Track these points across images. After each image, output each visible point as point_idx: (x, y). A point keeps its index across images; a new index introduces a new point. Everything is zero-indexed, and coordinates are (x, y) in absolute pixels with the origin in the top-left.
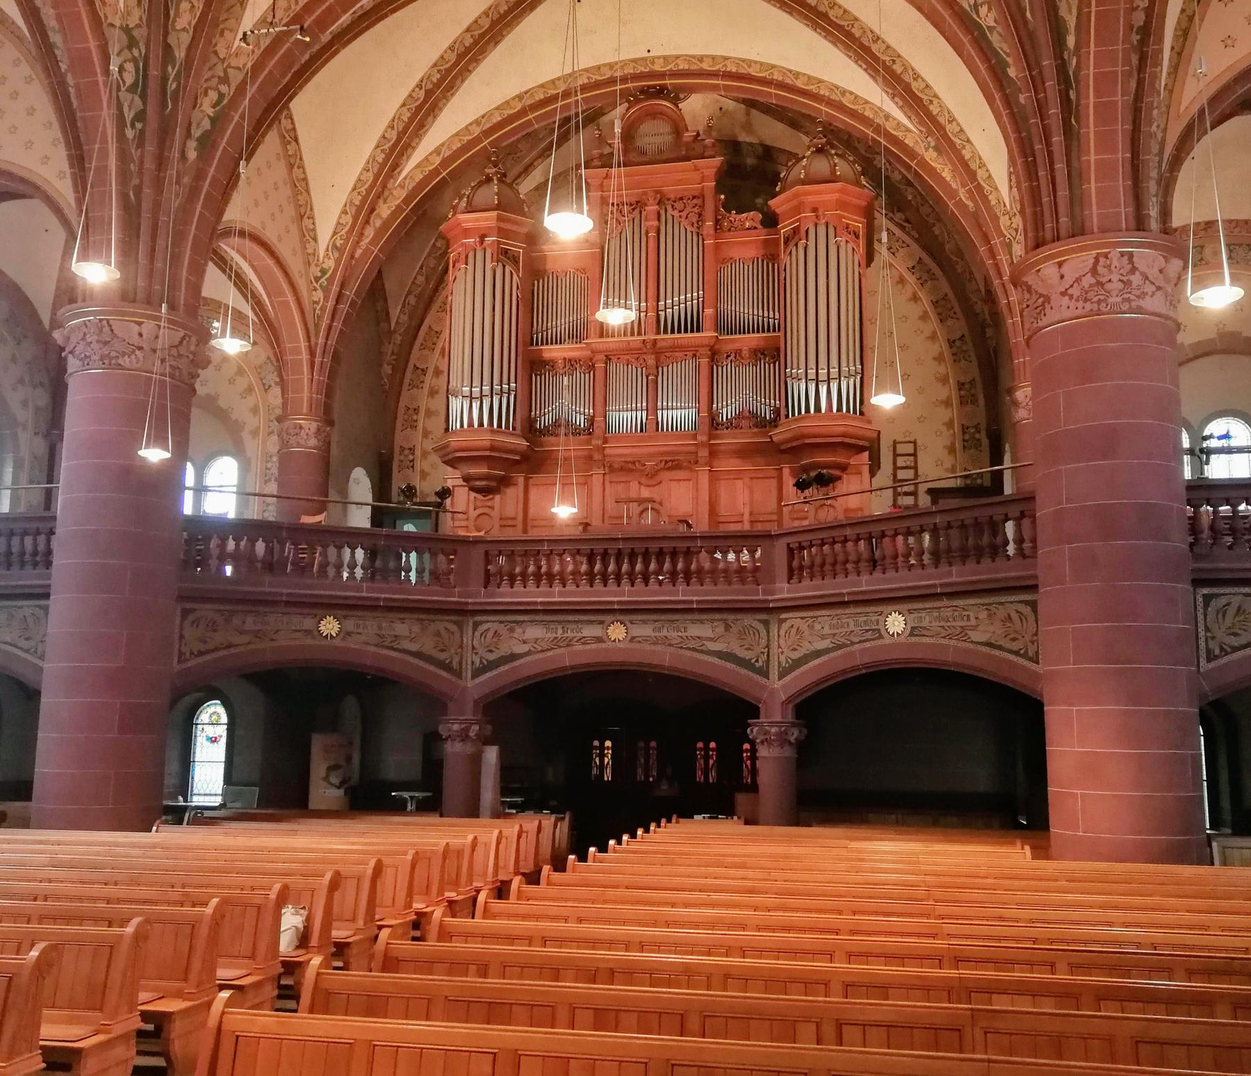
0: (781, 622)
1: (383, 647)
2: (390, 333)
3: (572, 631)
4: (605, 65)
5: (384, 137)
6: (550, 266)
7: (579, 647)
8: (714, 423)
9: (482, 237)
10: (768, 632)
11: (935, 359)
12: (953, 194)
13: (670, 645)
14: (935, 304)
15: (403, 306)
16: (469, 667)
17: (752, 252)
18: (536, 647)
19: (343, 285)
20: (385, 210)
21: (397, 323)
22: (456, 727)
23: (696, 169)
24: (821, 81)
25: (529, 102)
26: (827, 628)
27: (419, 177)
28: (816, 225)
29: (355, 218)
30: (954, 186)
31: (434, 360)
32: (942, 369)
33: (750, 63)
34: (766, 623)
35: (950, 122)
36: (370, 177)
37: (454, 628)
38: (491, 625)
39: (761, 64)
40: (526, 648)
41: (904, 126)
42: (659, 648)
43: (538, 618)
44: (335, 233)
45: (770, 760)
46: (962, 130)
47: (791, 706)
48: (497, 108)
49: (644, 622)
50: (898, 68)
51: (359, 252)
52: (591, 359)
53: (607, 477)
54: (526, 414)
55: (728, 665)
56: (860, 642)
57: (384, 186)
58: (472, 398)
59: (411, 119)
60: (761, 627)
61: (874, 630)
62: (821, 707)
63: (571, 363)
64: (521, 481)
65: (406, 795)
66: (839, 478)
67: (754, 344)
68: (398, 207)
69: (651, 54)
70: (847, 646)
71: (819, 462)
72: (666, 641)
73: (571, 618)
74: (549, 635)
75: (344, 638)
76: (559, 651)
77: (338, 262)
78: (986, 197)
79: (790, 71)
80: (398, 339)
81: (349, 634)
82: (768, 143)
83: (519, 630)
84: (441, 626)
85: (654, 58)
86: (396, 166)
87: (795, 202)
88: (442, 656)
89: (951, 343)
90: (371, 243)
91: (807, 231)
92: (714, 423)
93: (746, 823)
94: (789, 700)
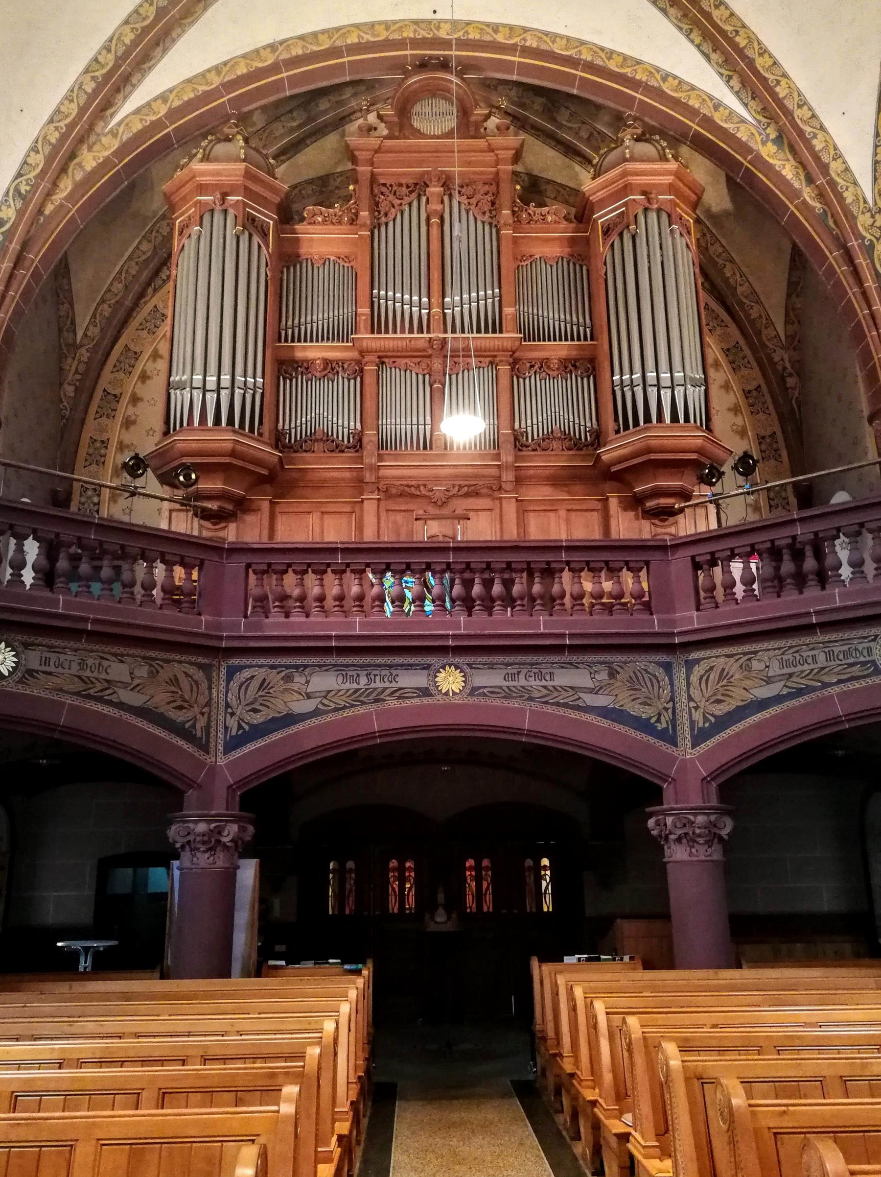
0: (690, 665)
1: (89, 697)
2: (74, 347)
3: (382, 680)
4: (380, 23)
5: (96, 60)
6: (303, 250)
7: (393, 703)
9: (224, 195)
10: (672, 684)
11: (729, 409)
12: (795, 194)
13: (531, 699)
15: (94, 316)
16: (221, 735)
17: (555, 251)
18: (323, 703)
19: (25, 245)
20: (89, 160)
21: (85, 335)
22: (202, 827)
23: (491, 149)
24: (638, 62)
25: (285, 56)
26: (775, 665)
27: (137, 126)
28: (646, 210)
29: (49, 160)
30: (796, 185)
31: (131, 384)
32: (739, 421)
33: (554, 37)
34: (668, 668)
35: (800, 106)
36: (73, 109)
37: (199, 675)
38: (256, 670)
39: (568, 39)
40: (309, 706)
42: (514, 704)
43: (329, 660)
44: (19, 175)
45: (688, 863)
46: (814, 116)
47: (714, 784)
48: (244, 56)
49: (491, 666)
50: (741, 41)
51: (49, 209)
52: (359, 362)
53: (382, 503)
55: (618, 727)
56: (840, 682)
57: (91, 128)
59: (135, 43)
60: (660, 672)
61: (863, 664)
62: (758, 782)
63: (330, 367)
64: (265, 506)
65: (77, 945)
66: (681, 510)
67: (563, 353)
68: (107, 160)
69: (438, 16)
70: (814, 689)
71: (661, 487)
72: (526, 694)
73: (379, 660)
74: (348, 685)
75: (20, 682)
76: (362, 710)
77: (20, 213)
78: (841, 194)
79: (602, 49)
80: (84, 354)
81: (30, 672)
82: (536, 173)
83: (299, 679)
84: (178, 669)
85: (440, 21)
86: (107, 106)
87: (620, 184)
88: (180, 717)
89: (747, 394)
90: (67, 199)
91: (636, 216)
92: (519, 442)
93: (648, 966)
94: (714, 775)
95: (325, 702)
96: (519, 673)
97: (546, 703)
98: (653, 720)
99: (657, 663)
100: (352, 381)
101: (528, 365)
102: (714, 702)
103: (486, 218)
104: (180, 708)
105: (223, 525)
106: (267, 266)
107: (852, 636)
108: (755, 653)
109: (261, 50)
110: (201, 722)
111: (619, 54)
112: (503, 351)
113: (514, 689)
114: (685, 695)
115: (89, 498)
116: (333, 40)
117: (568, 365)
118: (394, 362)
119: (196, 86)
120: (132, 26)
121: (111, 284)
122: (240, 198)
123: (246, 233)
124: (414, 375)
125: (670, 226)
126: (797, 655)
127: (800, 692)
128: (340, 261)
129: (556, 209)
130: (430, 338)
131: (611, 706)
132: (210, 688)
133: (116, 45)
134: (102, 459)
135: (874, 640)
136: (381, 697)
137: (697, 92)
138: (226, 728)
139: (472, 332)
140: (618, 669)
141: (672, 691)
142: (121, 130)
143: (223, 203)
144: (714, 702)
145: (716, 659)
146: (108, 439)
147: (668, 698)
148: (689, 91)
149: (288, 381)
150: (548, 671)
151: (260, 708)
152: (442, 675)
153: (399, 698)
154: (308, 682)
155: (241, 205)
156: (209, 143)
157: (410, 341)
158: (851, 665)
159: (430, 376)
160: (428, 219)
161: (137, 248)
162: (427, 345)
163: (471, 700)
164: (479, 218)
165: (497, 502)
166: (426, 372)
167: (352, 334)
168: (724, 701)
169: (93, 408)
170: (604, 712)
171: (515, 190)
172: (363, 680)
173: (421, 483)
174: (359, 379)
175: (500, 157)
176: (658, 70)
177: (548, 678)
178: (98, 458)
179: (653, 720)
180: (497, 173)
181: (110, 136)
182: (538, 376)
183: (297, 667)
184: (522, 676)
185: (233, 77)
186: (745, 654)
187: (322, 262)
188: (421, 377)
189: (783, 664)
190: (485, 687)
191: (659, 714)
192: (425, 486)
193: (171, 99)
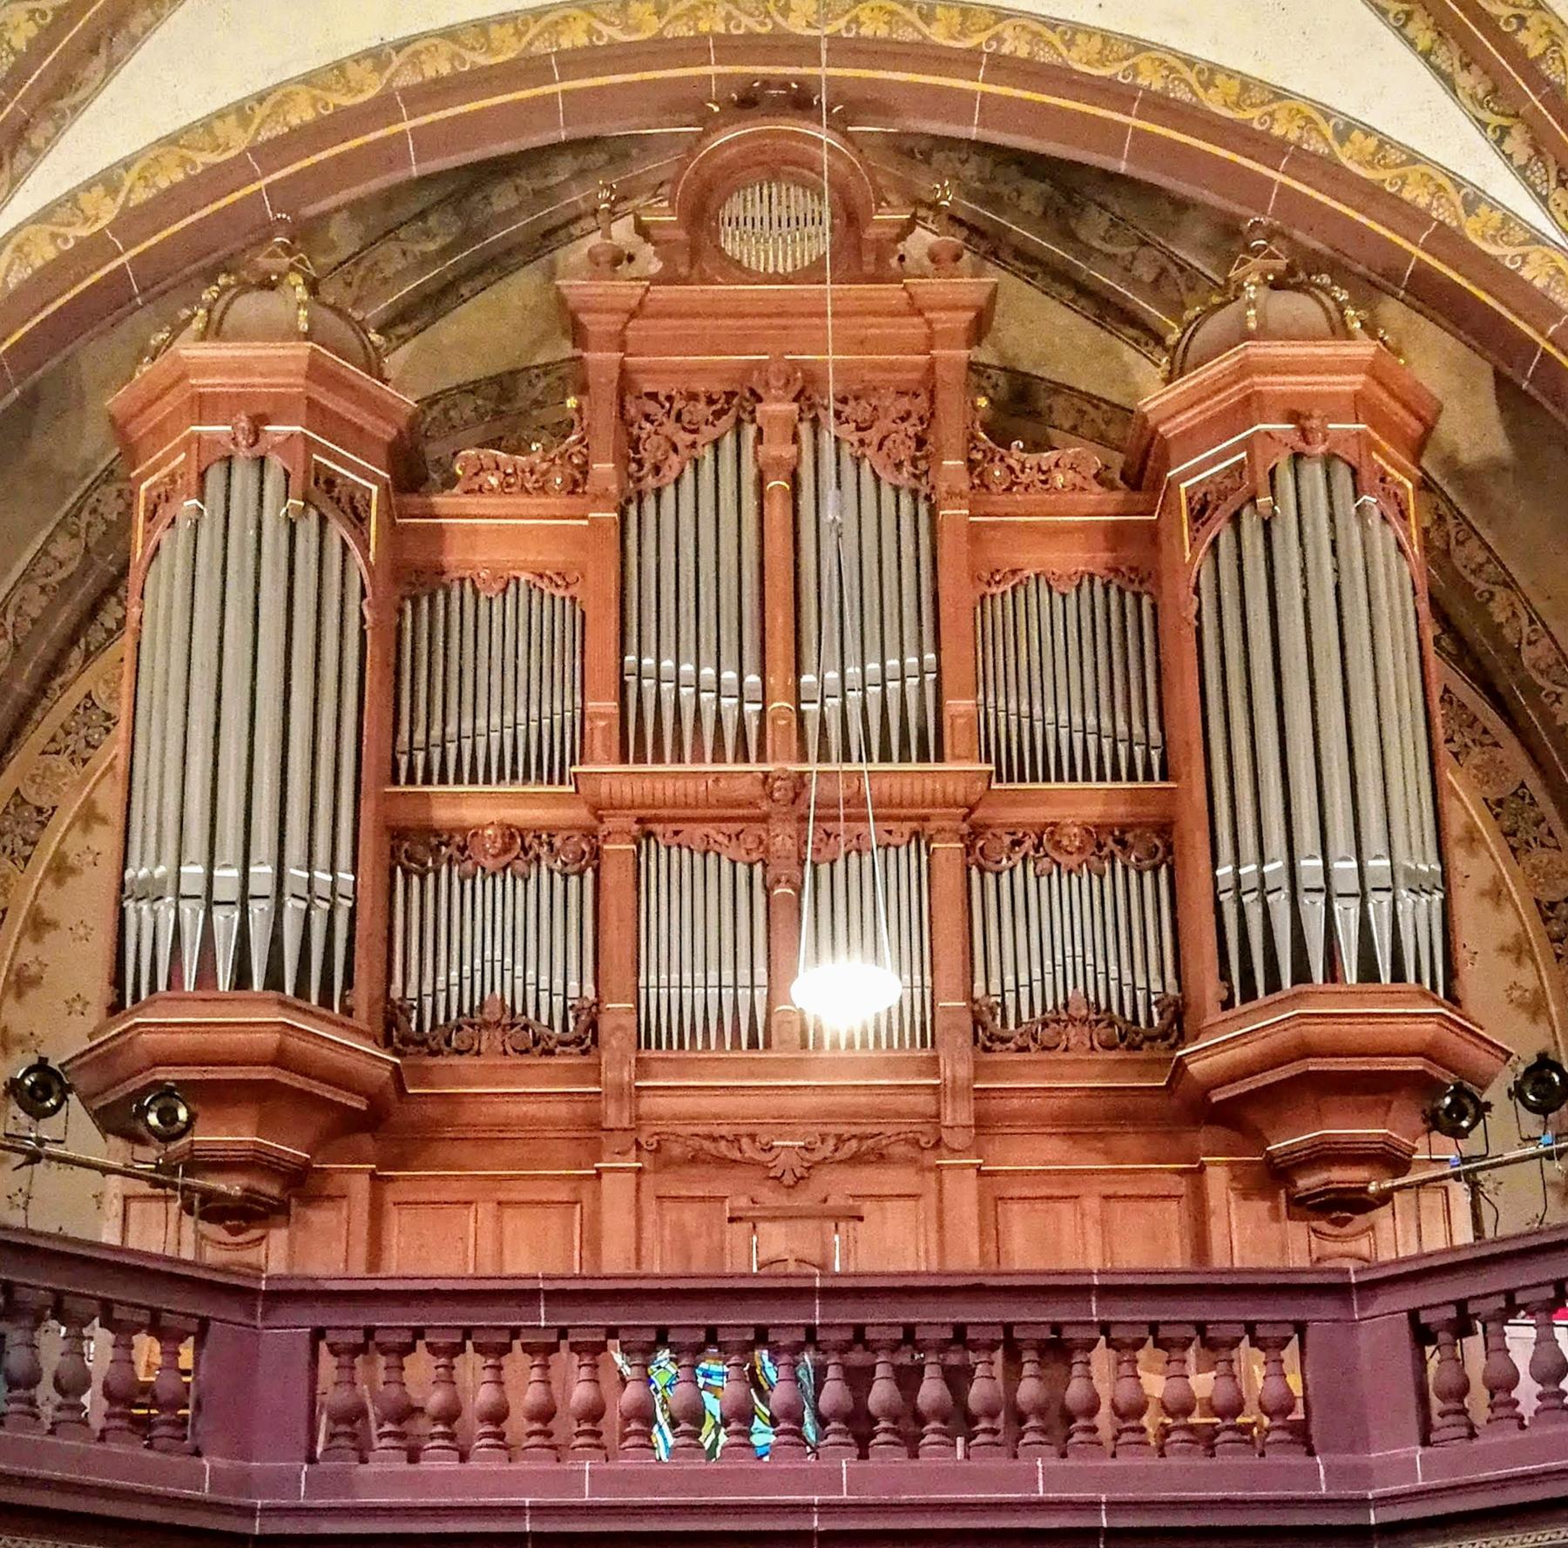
8: (984, 1030)
9: (259, 422)
14: (1496, 807)
25: (408, 79)
39: (1106, 37)
41: (1527, 227)
48: (308, 80)
52: (590, 833)
53: (648, 1180)
54: (378, 991)
58: (210, 904)
59: (39, 47)
63: (519, 844)
64: (360, 1186)
67: (1093, 812)
79: (1190, 62)
82: (1025, 366)
87: (1233, 394)
91: (1272, 473)
101: (1007, 840)
105: (255, 1233)
109: (349, 63)
111: (1231, 74)
112: (947, 805)
116: (525, 40)
117: (1106, 840)
118: (676, 833)
122: (298, 429)
123: (313, 514)
128: (544, 584)
130: (766, 775)
149: (415, 880)
155: (301, 446)
156: (220, 294)
157: (717, 780)
159: (765, 866)
160: (761, 481)
161: (44, 551)
162: (758, 790)
164: (887, 477)
165: (931, 1177)
166: (755, 856)
167: (573, 763)
171: (975, 408)
174: (589, 874)
176: (1327, 113)
182: (1031, 867)
185: (281, 130)
187: (498, 586)
188: (742, 869)
193: (128, 184)
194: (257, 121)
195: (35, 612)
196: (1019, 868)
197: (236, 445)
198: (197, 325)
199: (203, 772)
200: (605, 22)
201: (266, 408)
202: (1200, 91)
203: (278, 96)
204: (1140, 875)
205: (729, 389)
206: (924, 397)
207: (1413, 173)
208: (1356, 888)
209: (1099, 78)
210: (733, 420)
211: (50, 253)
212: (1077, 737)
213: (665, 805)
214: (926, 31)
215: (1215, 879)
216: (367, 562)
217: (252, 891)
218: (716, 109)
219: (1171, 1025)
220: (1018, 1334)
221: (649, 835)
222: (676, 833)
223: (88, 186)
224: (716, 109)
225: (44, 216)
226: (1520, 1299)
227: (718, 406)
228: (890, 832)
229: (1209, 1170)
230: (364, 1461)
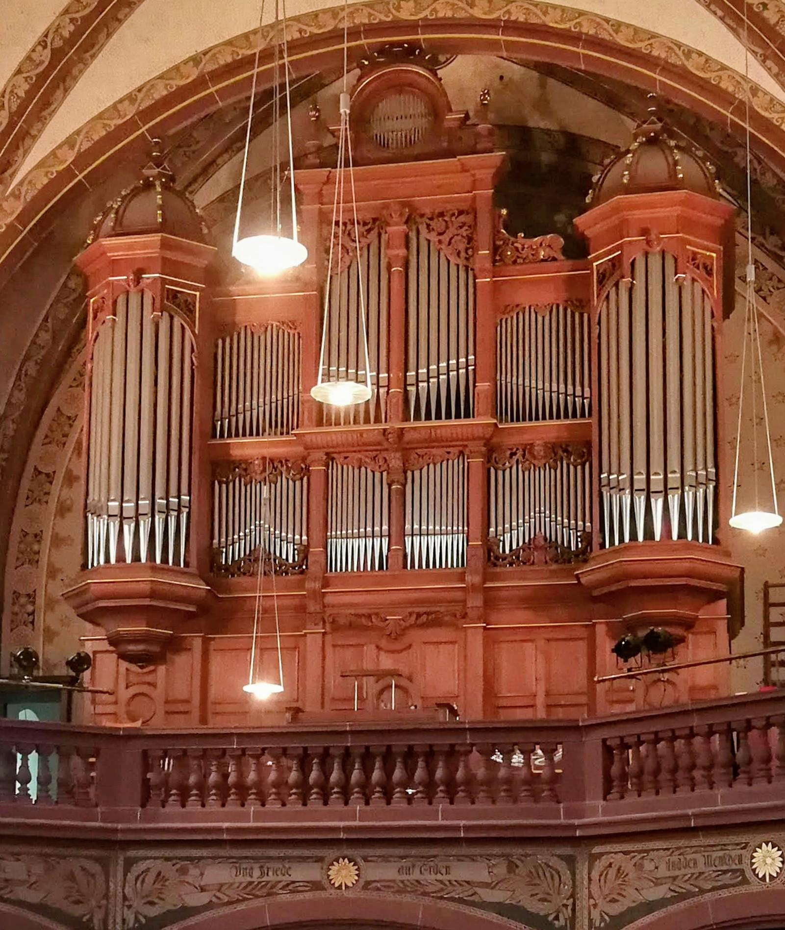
3: (275, 872)
4: (324, 11)
6: (241, 317)
7: (285, 897)
9: (138, 274)
13: (425, 894)
15: (18, 377)
17: (549, 296)
23: (464, 169)
24: (654, 36)
25: (210, 67)
26: (663, 866)
28: (646, 254)
31: (65, 459)
34: (571, 861)
37: (96, 868)
38: (151, 863)
40: (204, 898)
42: (407, 898)
43: (222, 852)
49: (385, 859)
52: (304, 459)
53: (328, 638)
54: (206, 543)
56: (714, 889)
59: (30, 95)
60: (562, 866)
61: (734, 871)
63: (273, 464)
64: (197, 644)
66: (682, 640)
67: (552, 436)
71: (650, 616)
79: (607, 20)
82: (574, 130)
83: (194, 871)
87: (614, 220)
91: (633, 264)
95: (218, 894)
96: (414, 866)
97: (442, 898)
98: (550, 918)
99: (559, 856)
100: (298, 483)
101: (509, 452)
102: (610, 901)
103: (461, 262)
104: (78, 902)
105: (152, 668)
106: (192, 351)
107: (727, 842)
108: (647, 851)
110: (98, 917)
111: (628, 26)
112: (474, 439)
113: (409, 884)
114: (587, 891)
115: (23, 606)
116: (268, 39)
117: (558, 451)
118: (346, 458)
119: (105, 122)
120: (25, 75)
121: (37, 335)
123: (166, 314)
124: (370, 474)
125: (676, 275)
126: (681, 857)
127: (681, 897)
128: (284, 327)
129: (551, 237)
130: (385, 430)
131: (508, 902)
132: (107, 881)
133: (10, 99)
134: (36, 557)
135: (744, 848)
136: (274, 890)
137: (730, 73)
138: (124, 920)
139: (440, 418)
140: (518, 863)
141: (574, 886)
142: (23, 190)
143: (138, 283)
144: (610, 901)
145: (613, 855)
146: (41, 531)
147: (569, 894)
148: (719, 70)
149: (224, 486)
150: (445, 864)
151: (156, 901)
152: (335, 868)
153: (292, 892)
154: (202, 874)
155: (159, 282)
156: (122, 201)
158: (725, 872)
159: (388, 473)
160: (389, 266)
161: (65, 285)
162: (381, 438)
163: (363, 895)
164: (453, 260)
165: (462, 634)
166: (382, 469)
167: (293, 429)
168: (618, 901)
169: (23, 491)
170: (500, 908)
171: (500, 216)
172: (256, 873)
173: (373, 611)
174: (305, 479)
175: (477, 176)
176: (679, 45)
177: (444, 871)
178: (32, 556)
179: (550, 918)
180: (474, 198)
181: (12, 199)
182: (520, 466)
183: (190, 859)
184: (417, 871)
186: (640, 852)
187: (263, 329)
188: (378, 475)
189: (670, 866)
190: (378, 882)
191: (558, 912)
192: (377, 614)
194: (139, 101)
195: (62, 317)
196: (514, 468)
197: (129, 285)
198: (110, 223)
199: (118, 451)
200: (307, 25)
201: (140, 266)
202: (614, 35)
203: (148, 86)
204: (575, 468)
205: (374, 216)
206: (471, 216)
207: (725, 74)
208: (662, 488)
209: (561, 29)
210: (376, 234)
211: (45, 181)
212: (547, 395)
213: (338, 446)
214: (471, 11)
215: (600, 479)
216: (193, 332)
217: (140, 512)
218: (366, 63)
219: (586, 547)
220: (435, 749)
221: (333, 459)
222: (346, 458)
223: (60, 147)
224: (366, 63)
225: (41, 165)
226: (643, 738)
227: (369, 226)
228: (449, 453)
229: (597, 626)
230: (164, 807)
